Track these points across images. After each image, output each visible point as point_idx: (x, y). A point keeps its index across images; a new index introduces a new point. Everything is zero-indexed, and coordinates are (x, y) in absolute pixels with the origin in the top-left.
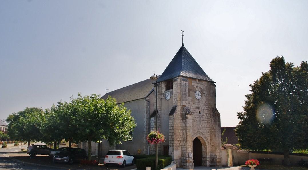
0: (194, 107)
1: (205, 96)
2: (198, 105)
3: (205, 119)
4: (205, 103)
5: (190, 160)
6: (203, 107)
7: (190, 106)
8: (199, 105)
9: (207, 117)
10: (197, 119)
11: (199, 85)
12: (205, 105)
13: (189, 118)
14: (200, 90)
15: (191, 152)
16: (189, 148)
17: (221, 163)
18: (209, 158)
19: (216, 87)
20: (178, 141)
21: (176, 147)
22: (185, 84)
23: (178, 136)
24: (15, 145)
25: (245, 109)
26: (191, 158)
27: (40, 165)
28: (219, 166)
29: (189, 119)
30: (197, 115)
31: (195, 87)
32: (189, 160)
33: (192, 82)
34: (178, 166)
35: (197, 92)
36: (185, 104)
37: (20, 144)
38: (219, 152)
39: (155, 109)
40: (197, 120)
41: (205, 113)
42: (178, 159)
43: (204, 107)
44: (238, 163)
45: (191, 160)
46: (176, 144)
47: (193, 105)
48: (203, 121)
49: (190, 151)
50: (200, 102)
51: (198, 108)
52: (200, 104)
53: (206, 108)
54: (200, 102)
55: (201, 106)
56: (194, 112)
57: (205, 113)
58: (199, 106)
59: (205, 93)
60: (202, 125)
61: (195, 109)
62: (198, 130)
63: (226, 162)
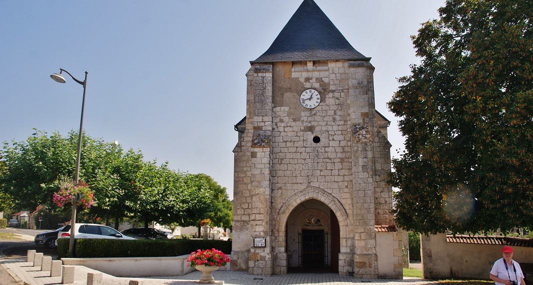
0: (295, 129)
1: (333, 97)
2: (310, 122)
3: (333, 156)
4: (335, 114)
5: (258, 254)
6: (327, 124)
7: (284, 127)
8: (314, 121)
9: (339, 150)
10: (304, 155)
11: (316, 75)
12: (334, 119)
13: (258, 153)
14: (317, 85)
15: (262, 234)
16: (256, 225)
17: (370, 267)
18: (345, 253)
19: (374, 74)
20: (244, 209)
21: (238, 224)
22: (263, 77)
23: (246, 198)
24: (299, 234)
25: (394, 112)
26: (262, 249)
27: (300, 261)
28: (362, 275)
29: (258, 156)
30: (305, 147)
31: (302, 80)
32: (255, 254)
33: (291, 72)
34: (428, 276)
35: (308, 91)
36: (263, 124)
37: (215, 228)
38: (363, 237)
39: (76, 130)
40: (305, 159)
41: (333, 140)
42: (242, 252)
43: (332, 126)
44: (451, 272)
45: (263, 254)
46: (239, 217)
47: (293, 124)
48: (328, 160)
49: (260, 232)
50: (318, 114)
51: (311, 129)
52: (317, 118)
53: (335, 128)
54: (315, 114)
55: (320, 123)
56: (297, 139)
57: (333, 140)
58: (313, 123)
59: (333, 91)
60: (321, 171)
61: (300, 134)
62: (309, 183)
63: (395, 266)
